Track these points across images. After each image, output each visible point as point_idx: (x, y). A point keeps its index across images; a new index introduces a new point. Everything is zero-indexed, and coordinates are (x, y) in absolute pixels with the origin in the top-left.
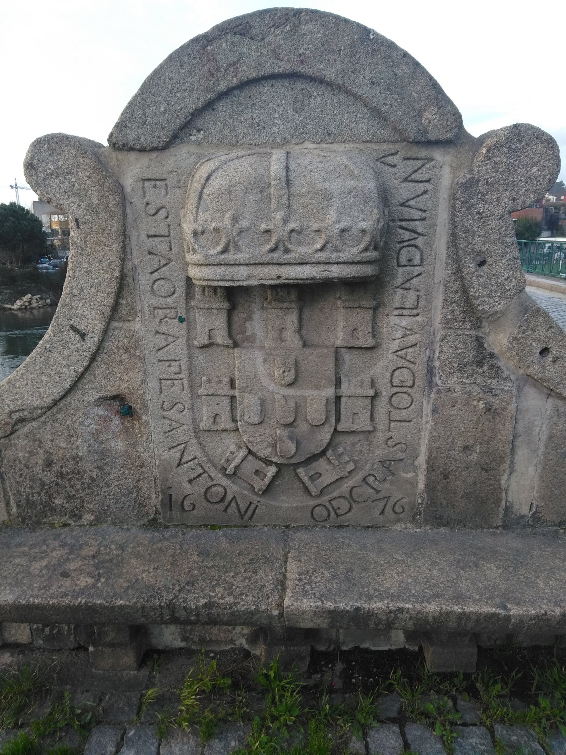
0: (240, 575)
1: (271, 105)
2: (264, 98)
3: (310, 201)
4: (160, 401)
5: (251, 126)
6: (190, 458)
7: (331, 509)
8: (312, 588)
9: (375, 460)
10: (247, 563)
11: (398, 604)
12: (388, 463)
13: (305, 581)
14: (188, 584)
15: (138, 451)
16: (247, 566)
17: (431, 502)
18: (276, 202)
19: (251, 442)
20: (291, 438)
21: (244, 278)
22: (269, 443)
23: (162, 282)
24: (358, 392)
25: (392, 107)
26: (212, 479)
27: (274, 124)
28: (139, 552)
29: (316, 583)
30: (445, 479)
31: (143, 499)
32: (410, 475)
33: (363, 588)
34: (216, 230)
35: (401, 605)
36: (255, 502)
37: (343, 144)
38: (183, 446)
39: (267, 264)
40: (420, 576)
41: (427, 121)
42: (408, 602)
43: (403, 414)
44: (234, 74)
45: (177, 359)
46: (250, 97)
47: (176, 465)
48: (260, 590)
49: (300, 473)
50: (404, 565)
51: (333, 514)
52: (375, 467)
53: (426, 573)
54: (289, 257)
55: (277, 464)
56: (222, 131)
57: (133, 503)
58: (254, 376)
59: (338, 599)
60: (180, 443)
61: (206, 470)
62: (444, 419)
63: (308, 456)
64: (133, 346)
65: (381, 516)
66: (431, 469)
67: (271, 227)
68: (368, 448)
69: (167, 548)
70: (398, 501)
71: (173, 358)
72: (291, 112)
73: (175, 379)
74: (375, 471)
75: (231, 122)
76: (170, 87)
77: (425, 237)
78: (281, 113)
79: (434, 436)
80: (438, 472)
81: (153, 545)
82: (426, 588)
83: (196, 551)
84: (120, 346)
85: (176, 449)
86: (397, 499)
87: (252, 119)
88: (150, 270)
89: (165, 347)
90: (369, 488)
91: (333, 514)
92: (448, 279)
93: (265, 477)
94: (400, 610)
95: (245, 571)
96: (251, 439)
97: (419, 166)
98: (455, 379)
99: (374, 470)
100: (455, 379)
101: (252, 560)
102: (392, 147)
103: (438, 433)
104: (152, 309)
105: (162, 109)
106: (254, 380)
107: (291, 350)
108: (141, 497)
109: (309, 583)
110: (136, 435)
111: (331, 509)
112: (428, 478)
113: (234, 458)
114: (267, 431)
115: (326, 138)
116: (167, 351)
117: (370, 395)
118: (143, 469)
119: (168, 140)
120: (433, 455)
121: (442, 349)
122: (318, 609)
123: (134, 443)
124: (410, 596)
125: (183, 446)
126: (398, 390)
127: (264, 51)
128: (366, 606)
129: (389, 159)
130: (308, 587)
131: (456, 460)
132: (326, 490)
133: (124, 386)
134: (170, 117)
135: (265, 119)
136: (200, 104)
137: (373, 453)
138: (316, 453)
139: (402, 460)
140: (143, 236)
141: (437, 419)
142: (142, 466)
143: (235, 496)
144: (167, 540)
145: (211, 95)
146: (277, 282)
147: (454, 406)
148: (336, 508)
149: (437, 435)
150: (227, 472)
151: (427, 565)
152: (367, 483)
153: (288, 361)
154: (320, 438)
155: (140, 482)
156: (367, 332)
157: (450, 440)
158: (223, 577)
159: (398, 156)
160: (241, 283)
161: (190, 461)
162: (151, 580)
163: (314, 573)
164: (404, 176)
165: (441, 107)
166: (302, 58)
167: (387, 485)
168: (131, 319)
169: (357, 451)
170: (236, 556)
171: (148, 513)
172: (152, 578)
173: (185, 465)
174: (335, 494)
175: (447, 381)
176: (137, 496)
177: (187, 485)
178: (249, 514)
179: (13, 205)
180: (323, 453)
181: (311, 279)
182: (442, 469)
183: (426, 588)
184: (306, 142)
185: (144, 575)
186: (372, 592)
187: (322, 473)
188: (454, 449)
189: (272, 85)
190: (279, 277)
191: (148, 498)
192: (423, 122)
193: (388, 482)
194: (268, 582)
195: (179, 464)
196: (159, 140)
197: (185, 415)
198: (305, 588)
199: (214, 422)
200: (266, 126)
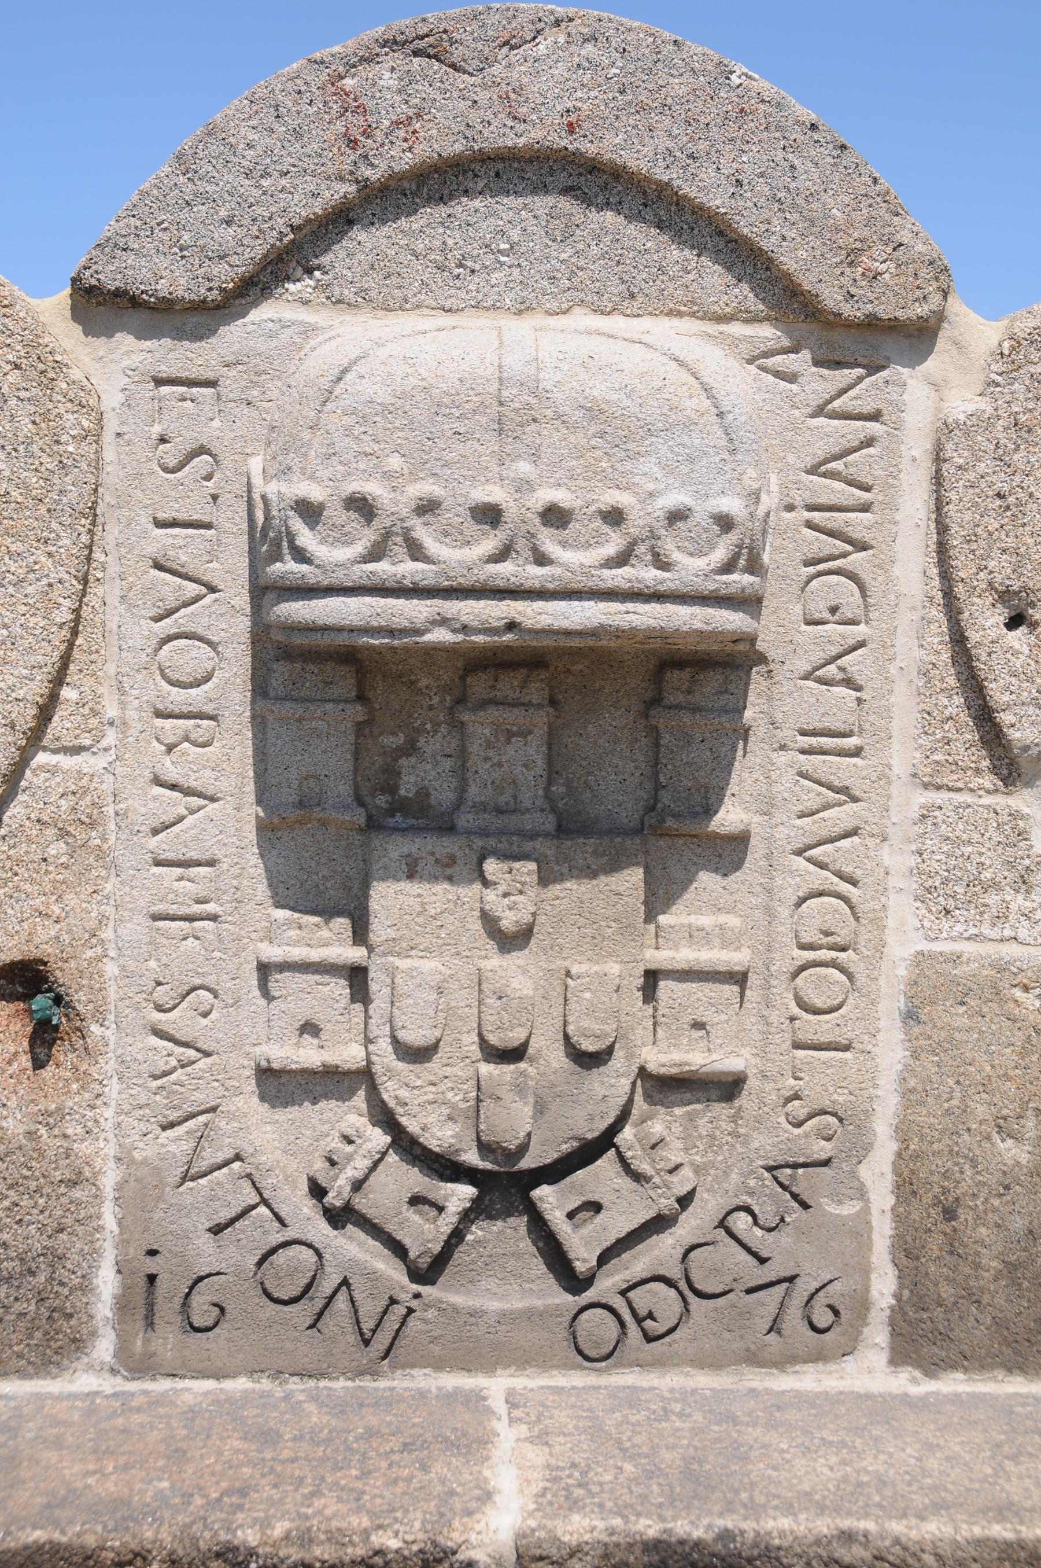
6: (220, 1157)
7: (627, 1317)
11: (838, 1521)
13: (570, 1481)
15: (65, 1136)
29: (601, 1484)
30: (948, 1220)
32: (849, 1209)
33: (737, 1492)
35: (846, 1523)
42: (866, 1516)
43: (821, 1027)
44: (405, 145)
52: (752, 1183)
54: (534, 574)
57: (32, 1307)
59: (669, 1514)
64: (83, 818)
66: (908, 1188)
70: (818, 1290)
77: (871, 552)
79: (912, 1091)
80: (928, 1199)
83: (234, 1429)
84: (45, 818)
86: (816, 1285)
87: (444, 248)
88: (154, 611)
89: (174, 824)
94: (847, 1537)
99: (751, 1193)
108: (62, 1284)
111: (627, 1317)
112: (898, 1217)
116: (178, 835)
118: (77, 1194)
120: (912, 1147)
122: (614, 1538)
127: (483, 96)
128: (749, 1526)
130: (579, 1492)
131: (974, 1163)
133: (46, 931)
137: (745, 1144)
139: (826, 1163)
142: (74, 1183)
148: (642, 1312)
154: (601, 1091)
161: (220, 1167)
164: (815, 402)
165: (901, 245)
166: (573, 118)
167: (784, 1239)
168: (87, 742)
171: (74, 1340)
177: (205, 1243)
179: (110, 336)
182: (937, 1190)
186: (761, 1499)
188: (969, 1130)
196: (208, 285)
198: (571, 1493)
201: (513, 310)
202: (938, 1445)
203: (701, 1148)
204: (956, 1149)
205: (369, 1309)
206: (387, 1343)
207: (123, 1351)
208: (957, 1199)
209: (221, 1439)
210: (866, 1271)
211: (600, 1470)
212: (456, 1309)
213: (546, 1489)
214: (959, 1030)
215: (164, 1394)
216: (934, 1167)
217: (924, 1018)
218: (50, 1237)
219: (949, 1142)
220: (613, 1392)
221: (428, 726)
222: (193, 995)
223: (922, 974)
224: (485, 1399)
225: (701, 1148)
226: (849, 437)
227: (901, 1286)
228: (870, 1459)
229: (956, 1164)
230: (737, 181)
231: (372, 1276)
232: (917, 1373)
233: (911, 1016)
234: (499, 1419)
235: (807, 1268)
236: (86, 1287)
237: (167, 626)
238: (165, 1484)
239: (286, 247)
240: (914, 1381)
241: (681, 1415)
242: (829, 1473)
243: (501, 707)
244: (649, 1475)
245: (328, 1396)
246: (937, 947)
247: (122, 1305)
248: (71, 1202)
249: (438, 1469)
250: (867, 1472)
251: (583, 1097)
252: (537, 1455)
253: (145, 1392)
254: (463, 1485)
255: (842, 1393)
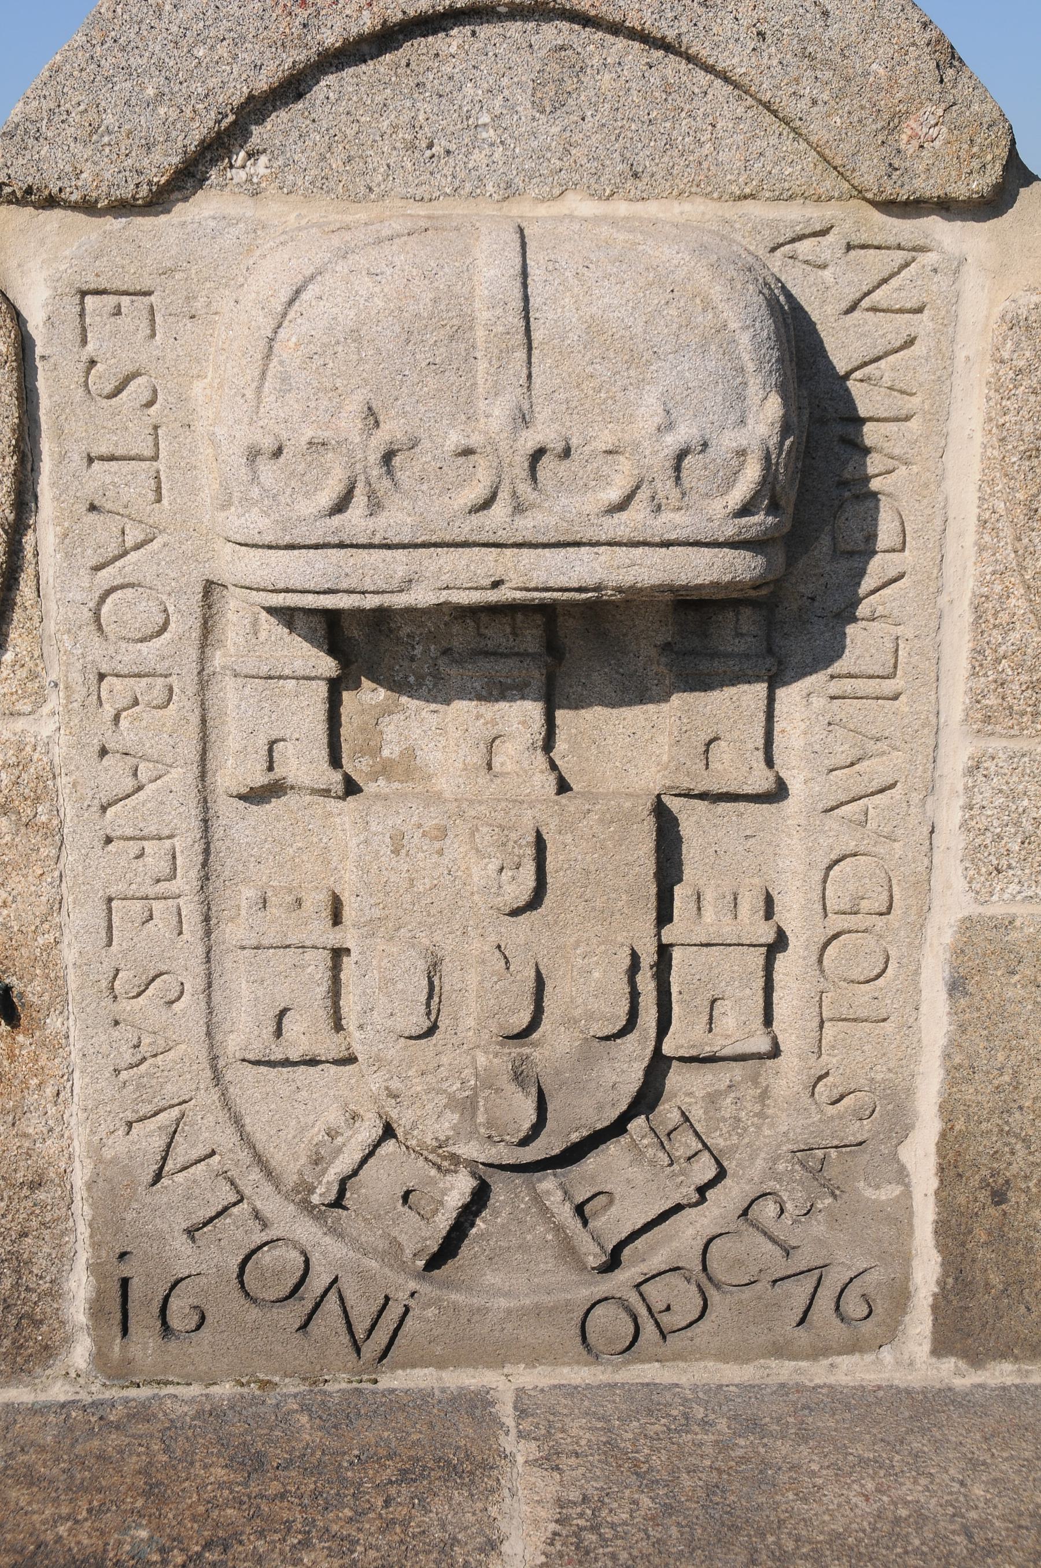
0: (372, 1515)
1: (469, 88)
2: (447, 69)
3: (589, 369)
4: (107, 968)
5: (411, 147)
6: (195, 1154)
7: (643, 1311)
8: (604, 1541)
9: (779, 1146)
10: (391, 1482)
12: (820, 1153)
13: (581, 1522)
14: (208, 1546)
15: (26, 1135)
16: (393, 1491)
17: (956, 1279)
18: (492, 370)
19: (396, 1097)
20: (518, 1077)
21: (395, 584)
22: (451, 1097)
23: (129, 592)
24: (728, 931)
25: (814, 102)
26: (265, 1225)
27: (474, 145)
28: (29, 1467)
29: (613, 1526)
30: (998, 1204)
31: (34, 1297)
32: (889, 1192)
33: (763, 1536)
34: (316, 445)
36: (403, 1296)
37: (676, 203)
38: (175, 1112)
39: (465, 544)
40: (934, 1501)
41: (915, 143)
45: (166, 832)
46: (408, 65)
47: (149, 1178)
48: (442, 1551)
49: (548, 1192)
50: (882, 1473)
51: (648, 1328)
53: (951, 1493)
54: (526, 526)
55: (472, 1165)
56: (323, 158)
58: (406, 885)
60: (164, 1103)
61: (247, 1191)
62: (984, 1011)
63: (575, 1137)
65: (801, 1332)
67: (475, 440)
68: (757, 1108)
69: (121, 1452)
71: (152, 829)
72: (525, 110)
73: (156, 898)
74: (780, 1181)
75: (350, 133)
76: (174, 29)
78: (497, 113)
81: (73, 1445)
82: (953, 1532)
83: (219, 1455)
85: (152, 1124)
89: (128, 796)
90: (761, 1239)
91: (648, 1328)
92: (985, 590)
93: (435, 1212)
95: (387, 1503)
96: (395, 1085)
97: (896, 265)
98: (1013, 888)
100: (1013, 888)
101: (403, 1472)
102: (816, 215)
103: (969, 1057)
104: (93, 678)
105: (151, 92)
106: (408, 897)
107: (522, 802)
108: (28, 1289)
109: (594, 1528)
110: (25, 1082)
111: (643, 1311)
113: (339, 1150)
114: (445, 1060)
115: (628, 185)
117: (762, 941)
118: (41, 1195)
119: (163, 180)
120: (957, 1128)
121: (971, 798)
123: (15, 1107)
124: (906, 1552)
125: (175, 1112)
126: (846, 926)
129: (804, 248)
130: (591, 1538)
131: (1026, 1141)
132: (627, 1252)
134: (173, 114)
135: (452, 128)
136: (262, 83)
137: (772, 1126)
138: (599, 1126)
140: (76, 457)
141: (963, 1011)
142: (36, 1185)
143: (336, 1280)
144: (117, 1428)
145: (298, 56)
146: (493, 597)
147: (1013, 973)
148: (658, 1306)
149: (966, 1063)
150: (315, 1199)
151: (952, 1471)
152: (755, 1225)
153: (514, 836)
154: (610, 1077)
155: (29, 1240)
156: (750, 746)
157: (1006, 1078)
158: (320, 1524)
159: (830, 238)
160: (387, 600)
162: (86, 1542)
163: (606, 1500)
165: (954, 104)
167: (818, 1227)
169: (724, 1120)
170: (351, 1463)
171: (46, 1347)
172: (90, 1537)
173: (180, 1178)
174: (657, 1262)
175: (992, 894)
176: (16, 1285)
177: (180, 1243)
178: (381, 1336)
180: (618, 1128)
181: (594, 590)
182: (985, 1172)
183: (953, 1532)
184: (570, 196)
185: (62, 1530)
187: (618, 1191)
188: (1021, 1108)
189: (474, 33)
190: (496, 584)
191: (49, 1293)
192: (903, 147)
193: (820, 1217)
194: (466, 1528)
195: (158, 1177)
197: (184, 1012)
199: (278, 1033)
200: (452, 147)
201: (496, 197)
202: (984, 1463)
203: (725, 1130)
204: (1007, 1128)
205: (362, 1315)
206: (385, 1340)
207: (100, 1358)
208: (1007, 1182)
209: (206, 1467)
210: (906, 1260)
211: (615, 1505)
212: (456, 1308)
213: (555, 1534)
214: (1011, 1001)
215: (145, 1405)
216: (981, 1149)
217: (971, 989)
218: (13, 1242)
219: (1000, 1122)
220: (629, 1390)
221: (412, 679)
222: (158, 980)
223: (969, 942)
224: (492, 1404)
225: (725, 1130)
226: (889, 336)
227: (946, 1274)
228: (909, 1485)
229: (1006, 1144)
230: (759, 33)
231: (363, 1276)
232: (962, 1364)
233: (956, 987)
234: (507, 1433)
235: (841, 1256)
236: (55, 1293)
237: (107, 576)
238: (144, 1534)
239: (227, 129)
240: (958, 1373)
241: (705, 1423)
242: (863, 1504)
243: (492, 658)
244: (668, 1510)
245: (323, 1402)
246: (988, 911)
247: (97, 1310)
248: (35, 1205)
249: (438, 1506)
250: (907, 1503)
251: (593, 1085)
252: (548, 1486)
253: (127, 1401)
254: (466, 1528)
255: (879, 1388)
